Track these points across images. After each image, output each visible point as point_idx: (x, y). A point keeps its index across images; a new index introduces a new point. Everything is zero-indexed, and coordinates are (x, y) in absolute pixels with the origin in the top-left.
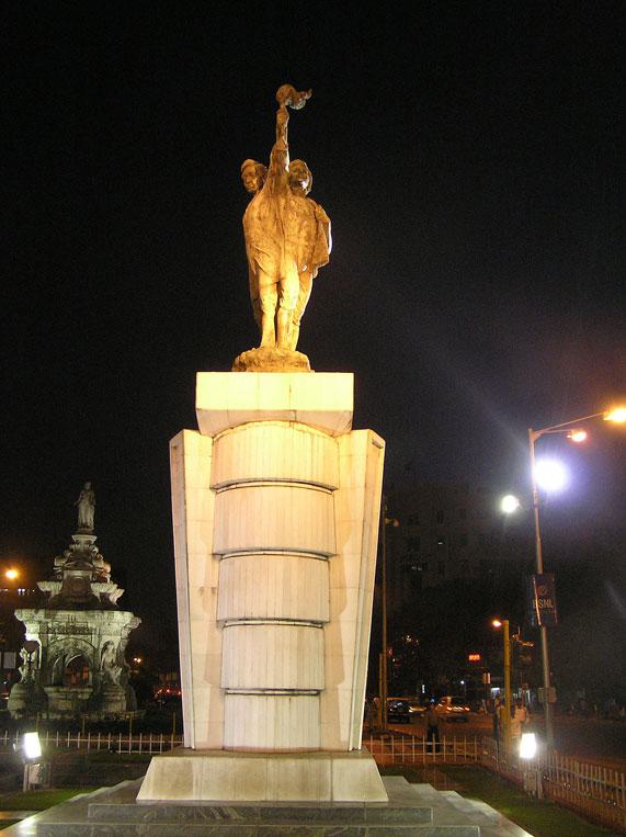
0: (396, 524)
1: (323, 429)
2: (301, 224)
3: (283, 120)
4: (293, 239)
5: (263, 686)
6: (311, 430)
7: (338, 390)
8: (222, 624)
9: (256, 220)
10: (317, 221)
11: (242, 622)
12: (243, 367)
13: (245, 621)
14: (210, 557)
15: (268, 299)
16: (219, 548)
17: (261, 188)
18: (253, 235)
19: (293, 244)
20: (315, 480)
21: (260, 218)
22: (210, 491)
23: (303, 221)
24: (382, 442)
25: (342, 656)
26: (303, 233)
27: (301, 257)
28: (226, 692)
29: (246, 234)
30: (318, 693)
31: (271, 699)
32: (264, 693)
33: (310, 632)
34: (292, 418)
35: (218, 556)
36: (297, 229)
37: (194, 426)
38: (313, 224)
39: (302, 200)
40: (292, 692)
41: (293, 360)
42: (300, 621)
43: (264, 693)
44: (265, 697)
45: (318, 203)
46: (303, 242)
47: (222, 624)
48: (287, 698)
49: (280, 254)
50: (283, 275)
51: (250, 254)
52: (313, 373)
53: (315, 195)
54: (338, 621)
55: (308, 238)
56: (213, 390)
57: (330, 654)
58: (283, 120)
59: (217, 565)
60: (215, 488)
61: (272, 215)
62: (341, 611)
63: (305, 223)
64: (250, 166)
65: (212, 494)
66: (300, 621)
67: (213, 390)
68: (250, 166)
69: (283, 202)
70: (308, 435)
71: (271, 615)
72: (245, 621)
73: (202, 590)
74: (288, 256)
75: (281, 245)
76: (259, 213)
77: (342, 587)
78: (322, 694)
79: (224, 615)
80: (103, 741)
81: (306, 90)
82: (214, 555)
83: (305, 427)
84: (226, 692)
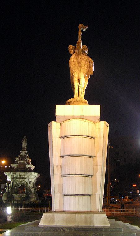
0: (112, 148)
1: (91, 121)
2: (85, 63)
3: (80, 34)
4: (83, 67)
5: (74, 193)
6: (88, 121)
7: (96, 110)
8: (63, 176)
9: (72, 62)
10: (90, 62)
11: (69, 175)
12: (69, 104)
13: (69, 175)
14: (60, 157)
15: (76, 84)
16: (62, 155)
17: (74, 53)
18: (71, 66)
19: (83, 69)
20: (89, 135)
21: (74, 62)
22: (59, 139)
23: (86, 62)
24: (108, 125)
25: (97, 185)
26: (86, 66)
27: (85, 72)
28: (64, 195)
29: (70, 66)
30: (90, 195)
31: (77, 197)
32: (75, 195)
33: (88, 178)
34: (83, 118)
35: (62, 157)
36: (84, 65)
37: (55, 120)
38: (89, 63)
39: (85, 56)
40: (83, 195)
41: (83, 101)
42: (85, 175)
43: (75, 195)
44: (75, 197)
45: (90, 57)
46: (86, 68)
47: (63, 176)
48: (81, 197)
49: (79, 72)
50: (80, 78)
51: (71, 72)
52: (89, 105)
53: (89, 55)
54: (96, 175)
55: (87, 67)
56: (60, 110)
57: (93, 184)
58: (80, 34)
59: (61, 159)
60: (61, 138)
61: (77, 61)
62: (97, 172)
63: (86, 63)
64: (71, 47)
65: (60, 139)
66: (85, 175)
67: (60, 110)
68: (71, 47)
69: (80, 57)
70: (87, 123)
71: (77, 174)
72: (69, 175)
73: (57, 166)
74: (81, 72)
75: (80, 69)
76: (73, 60)
77: (97, 166)
78: (91, 196)
79: (63, 173)
80: (29, 209)
81: (87, 25)
82: (61, 156)
83: (86, 121)
84: (64, 195)
